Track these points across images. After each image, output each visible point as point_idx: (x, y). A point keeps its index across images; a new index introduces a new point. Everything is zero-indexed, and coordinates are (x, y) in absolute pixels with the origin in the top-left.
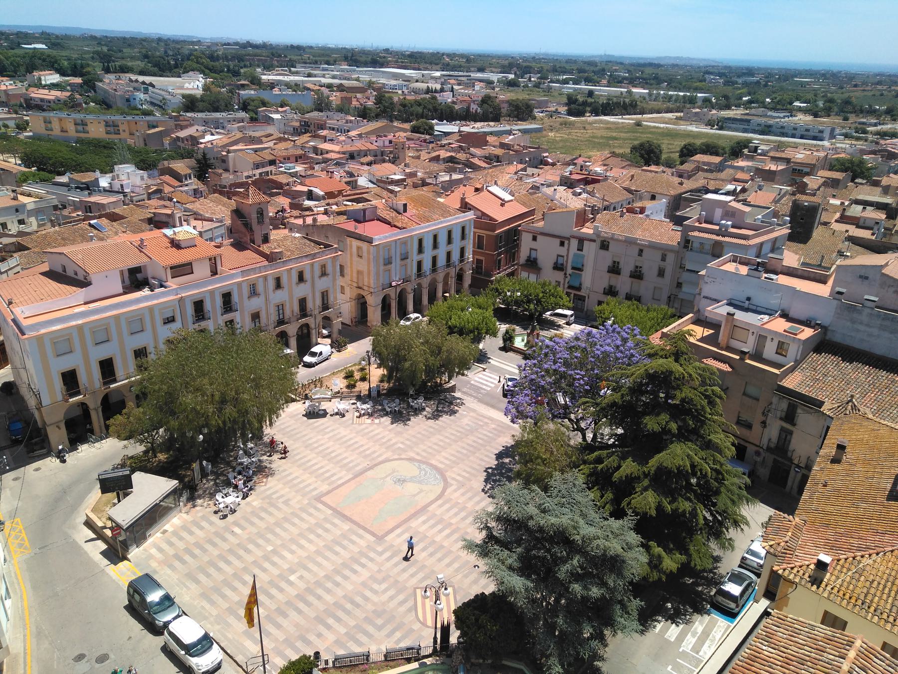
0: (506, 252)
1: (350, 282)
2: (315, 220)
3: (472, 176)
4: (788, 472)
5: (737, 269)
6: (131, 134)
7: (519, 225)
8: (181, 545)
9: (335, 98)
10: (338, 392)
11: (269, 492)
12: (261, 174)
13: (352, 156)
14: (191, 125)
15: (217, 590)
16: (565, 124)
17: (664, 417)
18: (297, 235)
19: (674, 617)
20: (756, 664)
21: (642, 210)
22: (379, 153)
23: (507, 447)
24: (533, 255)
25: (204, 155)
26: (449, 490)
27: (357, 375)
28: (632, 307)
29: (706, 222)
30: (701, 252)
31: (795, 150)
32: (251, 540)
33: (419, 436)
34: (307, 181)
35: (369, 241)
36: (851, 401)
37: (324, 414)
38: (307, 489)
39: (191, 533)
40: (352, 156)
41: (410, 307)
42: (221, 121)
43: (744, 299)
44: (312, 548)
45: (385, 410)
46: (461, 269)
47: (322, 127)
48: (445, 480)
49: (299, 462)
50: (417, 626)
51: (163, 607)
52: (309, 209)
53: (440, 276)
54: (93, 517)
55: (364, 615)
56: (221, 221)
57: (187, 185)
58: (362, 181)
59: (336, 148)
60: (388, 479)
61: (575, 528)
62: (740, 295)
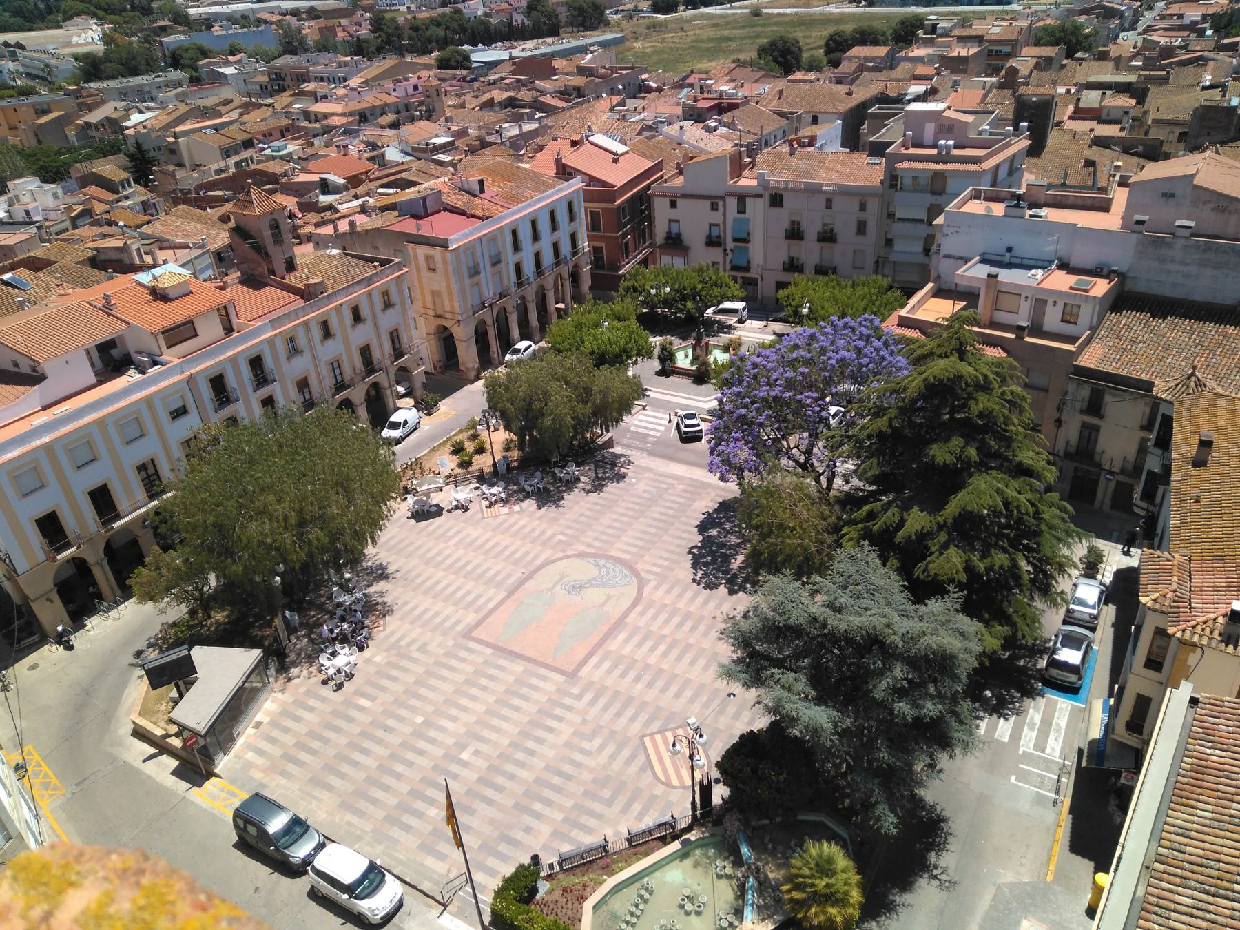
0: (632, 231)
1: (422, 310)
2: (352, 224)
3: (550, 124)
4: (1096, 483)
5: (988, 209)
6: (12, 128)
7: (648, 187)
8: (288, 740)
9: (310, 29)
10: (450, 476)
11: (393, 639)
12: (237, 164)
13: (363, 117)
14: (103, 102)
15: (361, 794)
16: (654, 26)
17: (956, 442)
18: (334, 252)
19: (999, 708)
20: (1206, 777)
21: (812, 141)
22: (402, 107)
23: (709, 514)
24: (675, 230)
25: (139, 146)
26: (647, 590)
27: (470, 447)
28: (830, 284)
29: (915, 146)
30: (915, 191)
31: (983, 22)
32: (388, 713)
33: (583, 519)
34: (311, 165)
35: (444, 244)
36: (1193, 374)
37: (438, 511)
38: (448, 624)
39: (298, 719)
40: (363, 117)
41: (515, 333)
42: (147, 89)
43: (1003, 251)
44: (480, 708)
45: (523, 490)
46: (576, 266)
47: (305, 78)
48: (637, 574)
49: (424, 587)
50: (659, 790)
51: (295, 836)
52: (330, 207)
53: (549, 281)
54: (143, 722)
55: (582, 789)
56: (203, 246)
57: (127, 198)
58: (392, 154)
59: (338, 108)
60: (558, 588)
61: (888, 626)
62: (996, 245)
